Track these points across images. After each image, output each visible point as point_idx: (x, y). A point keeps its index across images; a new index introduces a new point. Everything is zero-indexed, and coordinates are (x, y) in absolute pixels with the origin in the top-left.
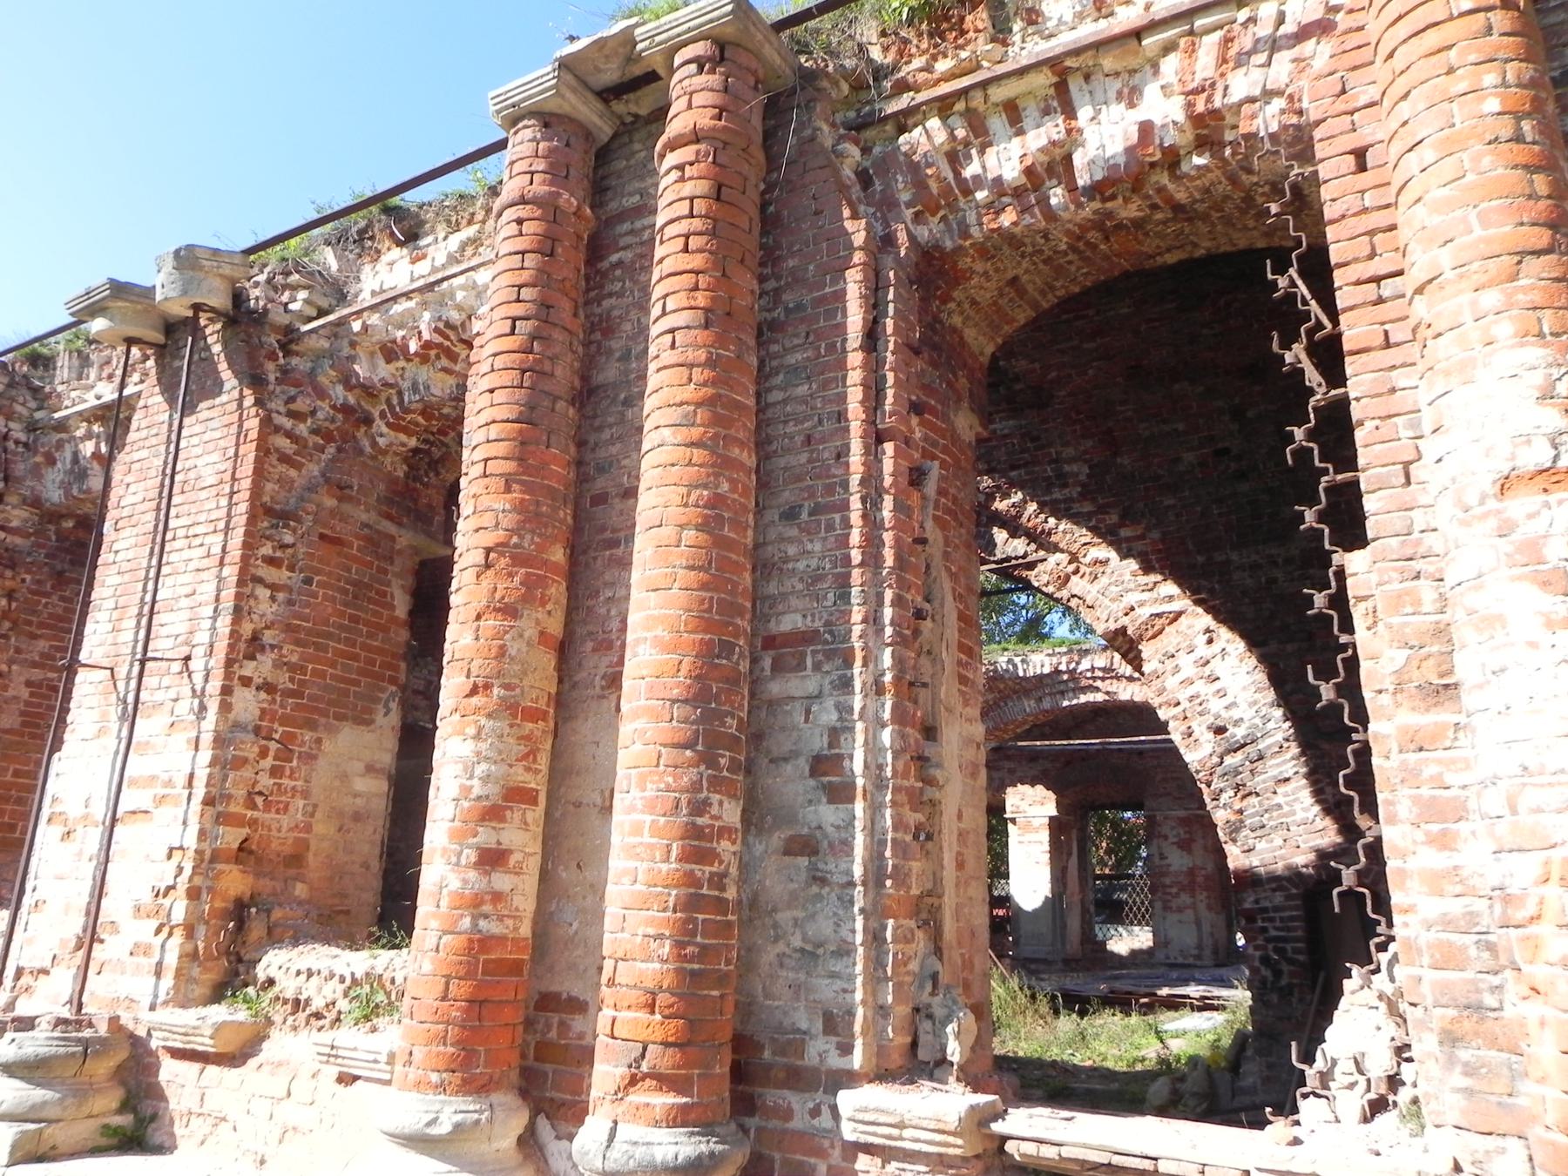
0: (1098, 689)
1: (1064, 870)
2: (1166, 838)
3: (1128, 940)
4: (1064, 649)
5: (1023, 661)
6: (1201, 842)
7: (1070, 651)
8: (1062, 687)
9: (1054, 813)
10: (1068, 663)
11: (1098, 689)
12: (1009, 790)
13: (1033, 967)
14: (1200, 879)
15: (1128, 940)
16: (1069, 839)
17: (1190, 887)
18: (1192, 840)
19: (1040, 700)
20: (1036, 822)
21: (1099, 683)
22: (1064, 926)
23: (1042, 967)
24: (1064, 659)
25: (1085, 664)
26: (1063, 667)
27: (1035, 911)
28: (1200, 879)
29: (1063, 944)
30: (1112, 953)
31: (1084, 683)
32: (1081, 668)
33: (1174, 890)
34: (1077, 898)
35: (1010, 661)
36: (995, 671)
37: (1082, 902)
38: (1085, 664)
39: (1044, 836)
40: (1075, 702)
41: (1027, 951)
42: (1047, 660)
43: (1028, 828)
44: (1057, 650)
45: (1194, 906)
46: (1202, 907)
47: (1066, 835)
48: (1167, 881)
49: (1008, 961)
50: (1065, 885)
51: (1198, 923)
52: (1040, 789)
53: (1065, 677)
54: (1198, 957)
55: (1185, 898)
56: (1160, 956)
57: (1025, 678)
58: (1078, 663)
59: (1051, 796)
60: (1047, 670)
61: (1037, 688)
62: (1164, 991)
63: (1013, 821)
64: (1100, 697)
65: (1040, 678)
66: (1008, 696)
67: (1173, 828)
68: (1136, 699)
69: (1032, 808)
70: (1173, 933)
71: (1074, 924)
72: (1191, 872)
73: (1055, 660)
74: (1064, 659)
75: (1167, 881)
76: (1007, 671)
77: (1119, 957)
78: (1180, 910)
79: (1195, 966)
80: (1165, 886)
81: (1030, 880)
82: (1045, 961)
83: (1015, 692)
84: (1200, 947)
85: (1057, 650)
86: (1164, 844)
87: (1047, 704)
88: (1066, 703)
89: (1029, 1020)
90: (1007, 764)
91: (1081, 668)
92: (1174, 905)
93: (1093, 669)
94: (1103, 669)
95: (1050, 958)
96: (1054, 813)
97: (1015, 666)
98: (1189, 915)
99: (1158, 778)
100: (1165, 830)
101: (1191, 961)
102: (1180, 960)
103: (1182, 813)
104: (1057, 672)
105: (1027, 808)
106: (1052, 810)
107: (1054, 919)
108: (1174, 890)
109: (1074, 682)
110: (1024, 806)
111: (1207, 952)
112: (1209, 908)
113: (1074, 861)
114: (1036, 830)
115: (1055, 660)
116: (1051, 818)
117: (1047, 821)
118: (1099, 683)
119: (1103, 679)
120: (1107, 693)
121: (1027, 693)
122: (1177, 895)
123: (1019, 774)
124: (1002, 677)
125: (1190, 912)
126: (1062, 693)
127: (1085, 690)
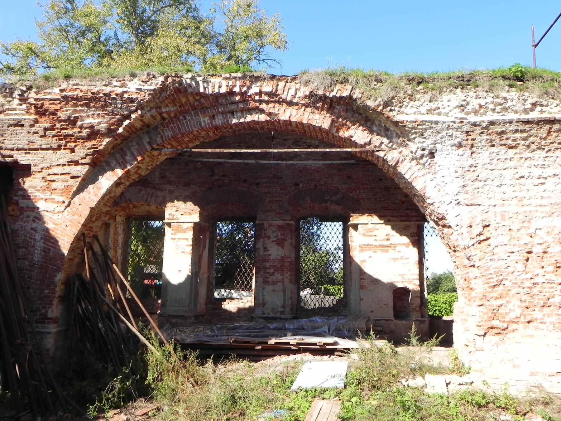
0: (262, 111)
1: (200, 257)
2: (269, 238)
3: (238, 301)
4: (239, 75)
5: (204, 81)
6: (289, 241)
7: (244, 77)
8: (233, 107)
9: (197, 219)
10: (241, 87)
11: (262, 111)
12: (169, 204)
13: (174, 321)
14: (287, 264)
15: (238, 301)
16: (204, 239)
17: (281, 270)
18: (285, 240)
19: (213, 117)
20: (185, 226)
21: (264, 106)
22: (197, 293)
23: (180, 321)
24: (238, 83)
25: (255, 89)
26: (237, 89)
27: (180, 285)
28: (287, 264)
29: (196, 305)
30: (226, 311)
31: (252, 104)
32: (251, 92)
33: (272, 271)
34: (206, 276)
35: (193, 78)
36: (181, 83)
37: (208, 277)
38: (255, 89)
39: (190, 235)
40: (242, 120)
41: (171, 310)
42: (224, 83)
43: (179, 229)
44: (234, 75)
45: (282, 281)
46: (287, 281)
47: (202, 232)
48: (268, 265)
49: (156, 316)
50: (200, 267)
51: (284, 291)
52: (190, 204)
53: (237, 98)
54: (282, 313)
55: (278, 276)
56: (259, 312)
57: (204, 96)
58: (249, 88)
59: (197, 209)
60: (223, 90)
61: (212, 106)
62: (272, 341)
63: (169, 225)
64: (263, 118)
65: (217, 96)
66: (187, 112)
67: (274, 232)
68: (293, 119)
69: (181, 219)
70: (268, 298)
71: (203, 291)
72: (283, 259)
73: (231, 83)
74: (238, 83)
75: (268, 265)
76: (190, 86)
77: (230, 313)
78: (274, 283)
79: (281, 319)
80: (265, 268)
81: (177, 263)
82: (183, 317)
83: (194, 108)
84: (284, 307)
85: (234, 75)
86: (268, 242)
87: (219, 121)
88: (234, 121)
89: (181, 378)
90: (168, 187)
91: (251, 92)
92: (270, 280)
93: (260, 93)
94: (269, 94)
95: (186, 314)
96: (197, 219)
97: (197, 83)
98: (279, 286)
99: (268, 200)
100: (269, 233)
101: (278, 315)
102: (271, 315)
103: (280, 223)
104: (231, 93)
105: (179, 217)
106: (196, 218)
107: (191, 289)
108: (272, 271)
109: (245, 103)
110: (177, 215)
111: (288, 309)
112: (291, 282)
113: (206, 253)
114: (185, 231)
115: (231, 83)
116: (195, 224)
117: (192, 225)
118: (264, 106)
119: (267, 103)
120: (270, 114)
121: (203, 109)
122: (273, 274)
123: (176, 194)
124: (186, 90)
125: (280, 285)
126: (232, 113)
127: (251, 111)
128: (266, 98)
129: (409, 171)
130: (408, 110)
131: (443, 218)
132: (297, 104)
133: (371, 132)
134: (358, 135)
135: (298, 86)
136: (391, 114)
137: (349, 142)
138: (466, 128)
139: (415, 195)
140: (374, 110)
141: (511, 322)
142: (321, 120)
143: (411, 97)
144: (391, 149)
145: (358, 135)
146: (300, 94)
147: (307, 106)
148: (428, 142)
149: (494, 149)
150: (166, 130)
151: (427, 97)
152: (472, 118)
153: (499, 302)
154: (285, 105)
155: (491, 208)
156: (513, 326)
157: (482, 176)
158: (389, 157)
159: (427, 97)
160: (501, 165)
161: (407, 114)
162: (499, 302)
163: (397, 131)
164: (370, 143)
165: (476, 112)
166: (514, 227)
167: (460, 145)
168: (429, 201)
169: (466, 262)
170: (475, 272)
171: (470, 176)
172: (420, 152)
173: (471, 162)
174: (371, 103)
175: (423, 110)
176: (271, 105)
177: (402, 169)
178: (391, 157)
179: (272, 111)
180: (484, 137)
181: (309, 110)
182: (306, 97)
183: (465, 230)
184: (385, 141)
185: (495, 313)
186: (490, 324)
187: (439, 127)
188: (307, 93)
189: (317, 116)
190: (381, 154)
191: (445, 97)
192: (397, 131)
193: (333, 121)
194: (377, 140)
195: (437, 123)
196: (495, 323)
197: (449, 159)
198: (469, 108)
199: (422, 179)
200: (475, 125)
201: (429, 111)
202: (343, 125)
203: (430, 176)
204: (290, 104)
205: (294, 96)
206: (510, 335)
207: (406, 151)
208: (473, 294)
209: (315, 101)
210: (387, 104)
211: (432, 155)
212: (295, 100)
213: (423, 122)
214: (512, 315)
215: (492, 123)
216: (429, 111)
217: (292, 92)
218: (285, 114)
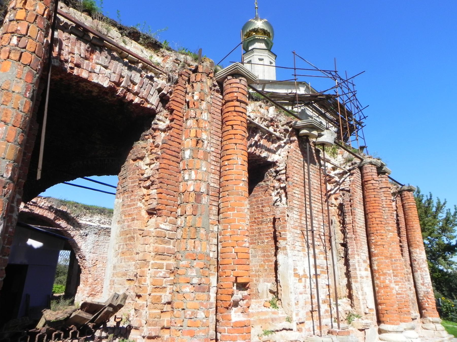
119: (31, 205)
128: (32, 204)
129: (77, 239)
130: (83, 219)
131: (85, 257)
132: (43, 208)
133: (68, 224)
134: (63, 223)
135: (45, 201)
136: (78, 220)
137: (59, 226)
138: (99, 229)
139: (75, 247)
140: (73, 218)
141: (97, 292)
142: (51, 216)
143: (85, 215)
144: (73, 230)
145: (63, 223)
146: (46, 205)
147: (46, 209)
148: (87, 231)
149: (105, 236)
150: (404, 318)
151: (90, 215)
152: (102, 226)
153: (95, 286)
154: (38, 208)
155: (102, 253)
156: (98, 293)
157: (100, 244)
158: (72, 234)
159: (90, 215)
160: (106, 241)
161: (83, 221)
162: (95, 286)
163: (77, 226)
164: (66, 227)
165: (103, 223)
166: (104, 262)
167: (96, 234)
168: (81, 251)
169: (88, 272)
170: (90, 275)
171: (96, 244)
172: (83, 234)
173: (97, 239)
174: (72, 215)
175: (88, 220)
176: (32, 206)
177: (75, 238)
178: (72, 233)
179: (32, 209)
180: (104, 232)
181: (47, 211)
182: (47, 206)
183: (90, 261)
184: (72, 227)
185: (93, 290)
186: (91, 293)
187: (92, 227)
188: (49, 206)
189: (50, 214)
190: (69, 232)
191: (95, 216)
192: (77, 226)
193: (55, 217)
194: (69, 227)
195: (91, 226)
196: (93, 293)
197: (91, 238)
198: (101, 222)
199: (81, 243)
200: (102, 228)
201: (89, 221)
202: (58, 219)
203: (83, 242)
204: (40, 207)
205: (43, 205)
206: (96, 296)
207: (78, 232)
208: (88, 283)
209: (50, 209)
210: (78, 216)
211: (86, 235)
212: (43, 207)
213: (87, 225)
214: (98, 290)
215: (107, 228)
216: (89, 221)
217: (43, 203)
218: (37, 211)
